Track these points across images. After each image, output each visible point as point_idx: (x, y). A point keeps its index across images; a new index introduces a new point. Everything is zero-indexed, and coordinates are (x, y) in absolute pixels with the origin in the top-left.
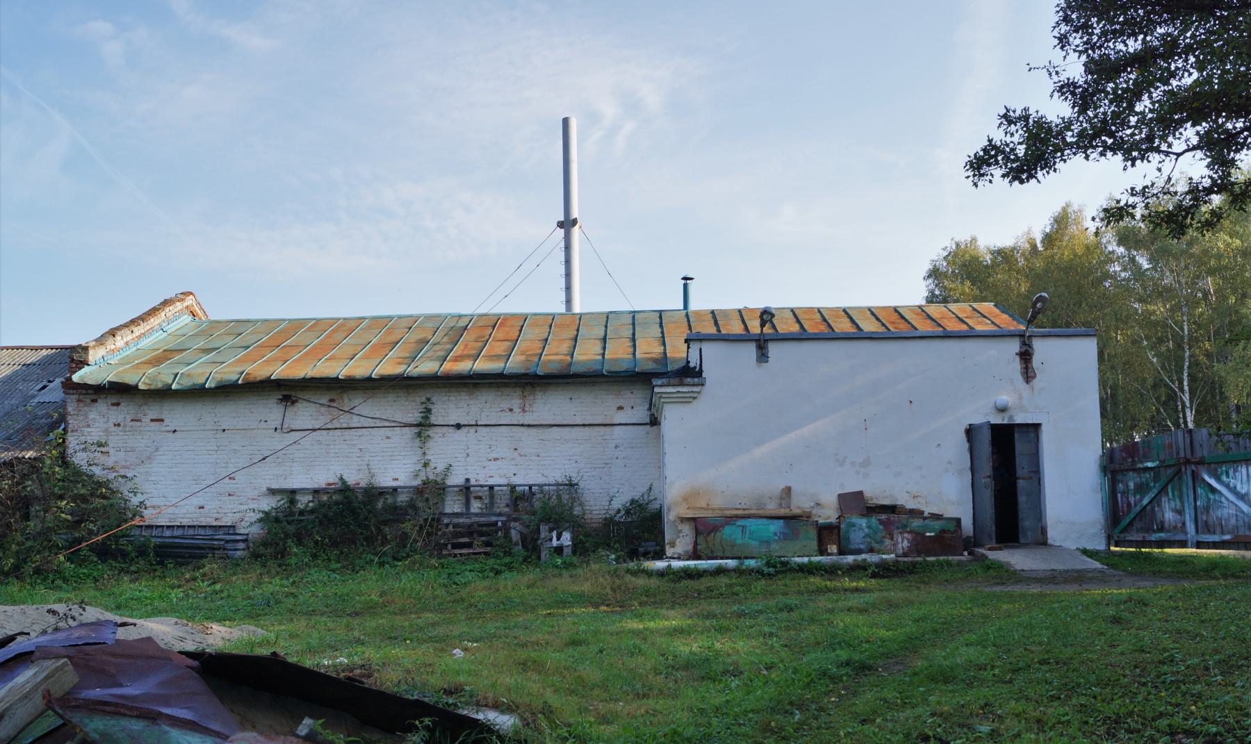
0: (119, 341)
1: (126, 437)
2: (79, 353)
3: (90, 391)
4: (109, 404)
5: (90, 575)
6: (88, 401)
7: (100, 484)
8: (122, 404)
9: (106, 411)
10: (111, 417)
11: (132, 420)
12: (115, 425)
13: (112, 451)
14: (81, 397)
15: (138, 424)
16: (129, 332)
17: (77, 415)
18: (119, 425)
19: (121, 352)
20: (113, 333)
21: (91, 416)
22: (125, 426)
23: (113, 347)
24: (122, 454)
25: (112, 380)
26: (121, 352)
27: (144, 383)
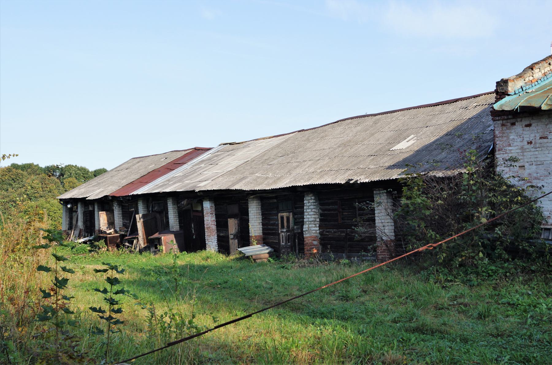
0: (537, 74)
1: (537, 153)
2: (501, 86)
3: (510, 117)
4: (524, 126)
5: (496, 272)
6: (509, 124)
7: (518, 193)
8: (533, 125)
9: (521, 132)
10: (525, 136)
11: (541, 138)
12: (528, 143)
13: (527, 165)
14: (504, 122)
15: (545, 140)
16: (546, 65)
17: (502, 137)
18: (531, 143)
19: (539, 82)
20: (531, 68)
21: (511, 137)
22: (535, 143)
23: (531, 78)
24: (534, 167)
25: (522, 105)
26: (539, 82)
27: (547, 104)
